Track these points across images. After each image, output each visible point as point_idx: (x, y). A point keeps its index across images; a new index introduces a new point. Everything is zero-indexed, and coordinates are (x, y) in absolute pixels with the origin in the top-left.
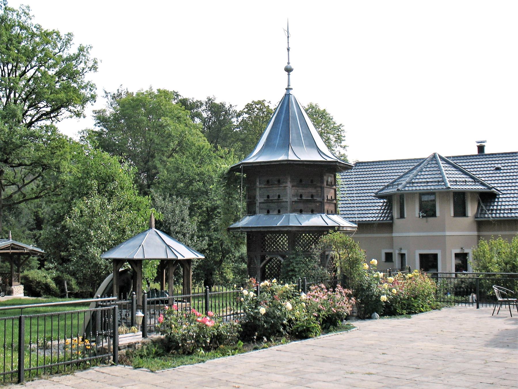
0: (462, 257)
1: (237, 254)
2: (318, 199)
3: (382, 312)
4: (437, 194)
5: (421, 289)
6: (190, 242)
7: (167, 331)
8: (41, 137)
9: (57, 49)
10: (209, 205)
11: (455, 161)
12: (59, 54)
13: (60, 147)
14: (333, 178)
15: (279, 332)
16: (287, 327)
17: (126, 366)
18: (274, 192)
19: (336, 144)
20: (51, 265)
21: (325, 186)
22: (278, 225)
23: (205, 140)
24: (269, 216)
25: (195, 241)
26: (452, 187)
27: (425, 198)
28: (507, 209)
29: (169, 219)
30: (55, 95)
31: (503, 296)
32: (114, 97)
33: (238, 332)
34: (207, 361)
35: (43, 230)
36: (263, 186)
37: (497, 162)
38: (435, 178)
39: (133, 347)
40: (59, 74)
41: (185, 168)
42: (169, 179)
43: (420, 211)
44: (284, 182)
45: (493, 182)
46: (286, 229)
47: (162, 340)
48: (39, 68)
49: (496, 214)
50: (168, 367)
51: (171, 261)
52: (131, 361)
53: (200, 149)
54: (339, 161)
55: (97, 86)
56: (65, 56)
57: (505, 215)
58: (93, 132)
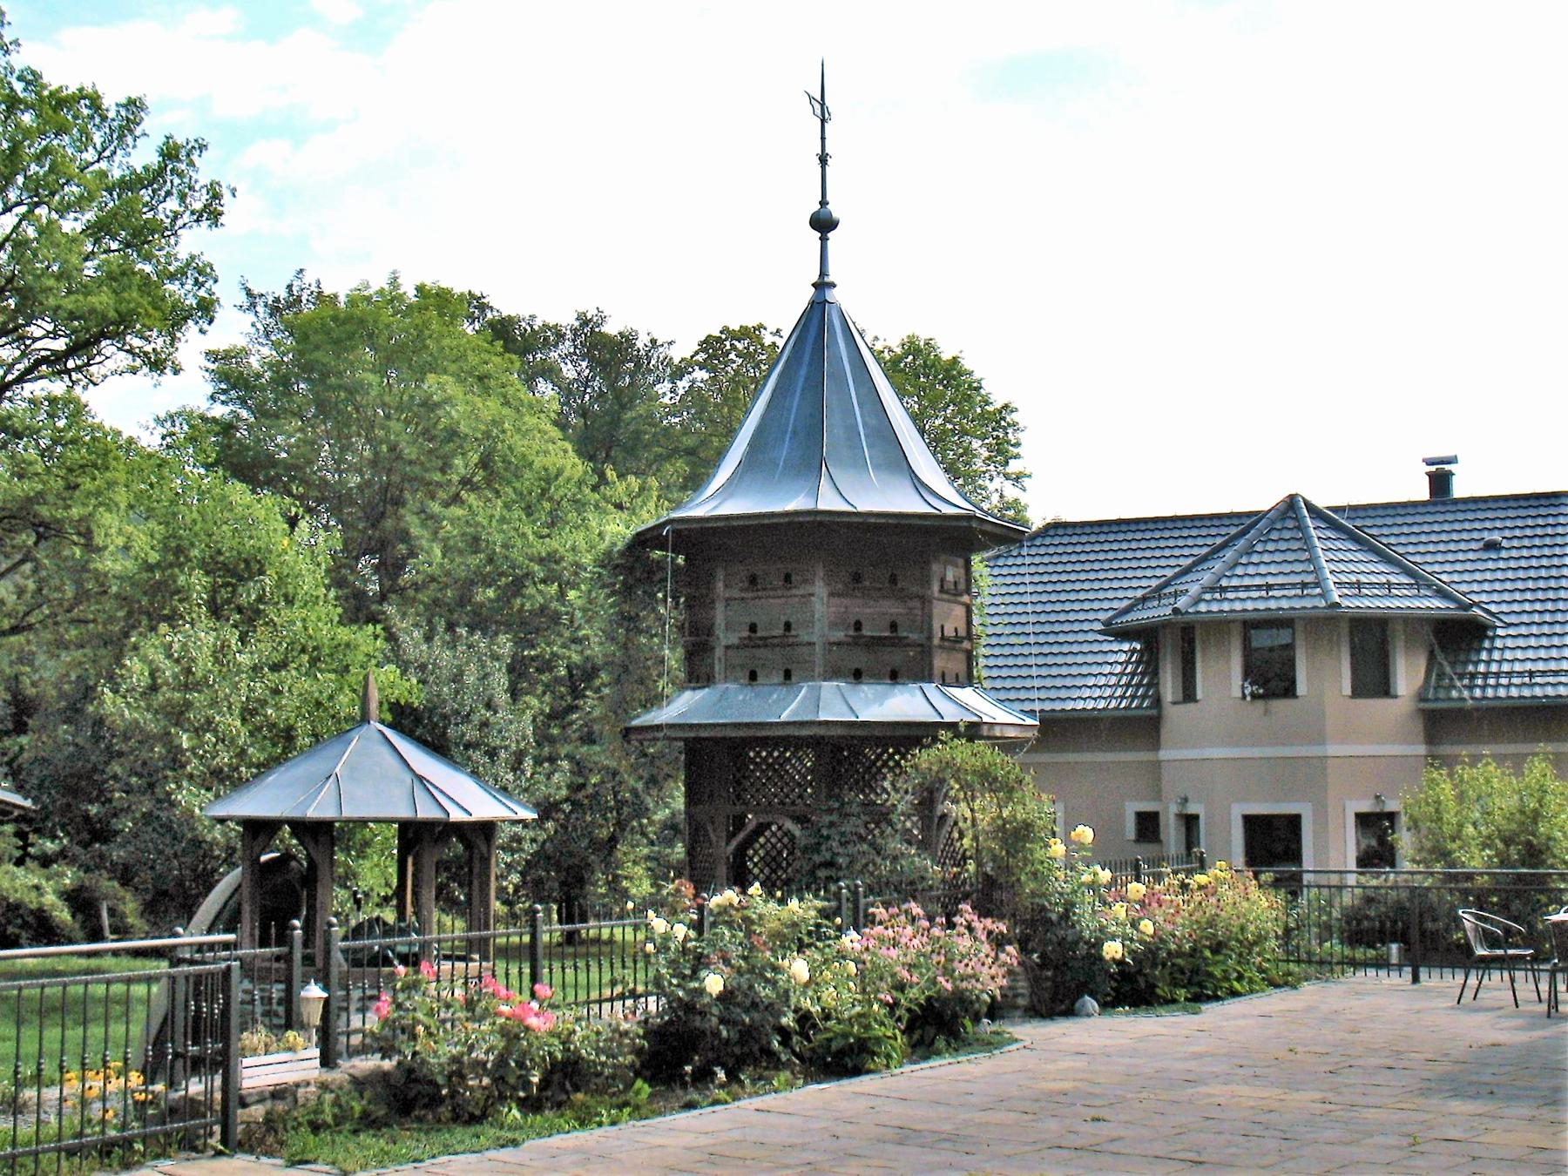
0: (1375, 824)
1: (661, 815)
2: (914, 636)
3: (1109, 995)
4: (1299, 627)
5: (1236, 923)
6: (510, 777)
7: (403, 1047)
8: (33, 433)
9: (90, 149)
10: (576, 658)
11: (1359, 523)
12: (96, 167)
13: (95, 466)
14: (962, 571)
15: (769, 1053)
16: (795, 1038)
17: (264, 1159)
18: (771, 611)
19: (992, 468)
20: (48, 844)
21: (936, 594)
22: (785, 717)
23: (565, 451)
24: (758, 689)
25: (529, 775)
26: (1345, 603)
27: (1262, 639)
28: (1520, 674)
29: (444, 701)
30: (81, 298)
31: (1491, 940)
32: (275, 309)
33: (639, 1052)
34: (526, 1144)
35: (30, 733)
36: (736, 593)
37: (1488, 525)
38: (1292, 575)
39: (290, 1099)
40: (97, 230)
41: (498, 538)
42: (448, 574)
43: (1245, 680)
44: (805, 581)
45: (1475, 587)
46: (805, 732)
47: (385, 1076)
48: (31, 211)
49: (1484, 688)
50: (399, 1160)
51: (429, 825)
52: (282, 1143)
53: (549, 479)
54: (979, 514)
55: (218, 272)
56: (117, 174)
57: (1514, 692)
58: (203, 418)
